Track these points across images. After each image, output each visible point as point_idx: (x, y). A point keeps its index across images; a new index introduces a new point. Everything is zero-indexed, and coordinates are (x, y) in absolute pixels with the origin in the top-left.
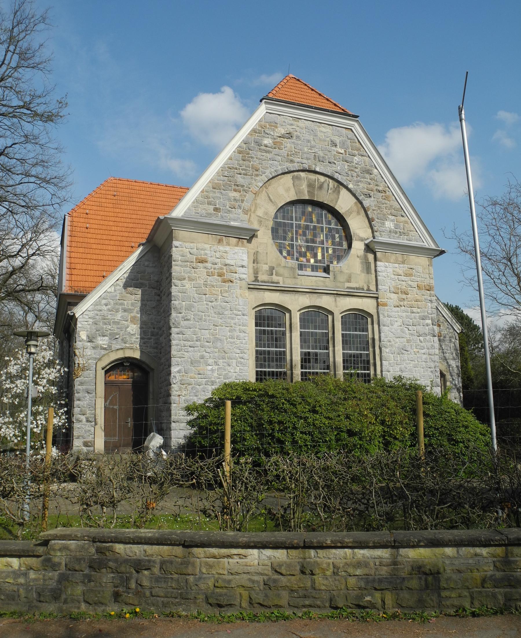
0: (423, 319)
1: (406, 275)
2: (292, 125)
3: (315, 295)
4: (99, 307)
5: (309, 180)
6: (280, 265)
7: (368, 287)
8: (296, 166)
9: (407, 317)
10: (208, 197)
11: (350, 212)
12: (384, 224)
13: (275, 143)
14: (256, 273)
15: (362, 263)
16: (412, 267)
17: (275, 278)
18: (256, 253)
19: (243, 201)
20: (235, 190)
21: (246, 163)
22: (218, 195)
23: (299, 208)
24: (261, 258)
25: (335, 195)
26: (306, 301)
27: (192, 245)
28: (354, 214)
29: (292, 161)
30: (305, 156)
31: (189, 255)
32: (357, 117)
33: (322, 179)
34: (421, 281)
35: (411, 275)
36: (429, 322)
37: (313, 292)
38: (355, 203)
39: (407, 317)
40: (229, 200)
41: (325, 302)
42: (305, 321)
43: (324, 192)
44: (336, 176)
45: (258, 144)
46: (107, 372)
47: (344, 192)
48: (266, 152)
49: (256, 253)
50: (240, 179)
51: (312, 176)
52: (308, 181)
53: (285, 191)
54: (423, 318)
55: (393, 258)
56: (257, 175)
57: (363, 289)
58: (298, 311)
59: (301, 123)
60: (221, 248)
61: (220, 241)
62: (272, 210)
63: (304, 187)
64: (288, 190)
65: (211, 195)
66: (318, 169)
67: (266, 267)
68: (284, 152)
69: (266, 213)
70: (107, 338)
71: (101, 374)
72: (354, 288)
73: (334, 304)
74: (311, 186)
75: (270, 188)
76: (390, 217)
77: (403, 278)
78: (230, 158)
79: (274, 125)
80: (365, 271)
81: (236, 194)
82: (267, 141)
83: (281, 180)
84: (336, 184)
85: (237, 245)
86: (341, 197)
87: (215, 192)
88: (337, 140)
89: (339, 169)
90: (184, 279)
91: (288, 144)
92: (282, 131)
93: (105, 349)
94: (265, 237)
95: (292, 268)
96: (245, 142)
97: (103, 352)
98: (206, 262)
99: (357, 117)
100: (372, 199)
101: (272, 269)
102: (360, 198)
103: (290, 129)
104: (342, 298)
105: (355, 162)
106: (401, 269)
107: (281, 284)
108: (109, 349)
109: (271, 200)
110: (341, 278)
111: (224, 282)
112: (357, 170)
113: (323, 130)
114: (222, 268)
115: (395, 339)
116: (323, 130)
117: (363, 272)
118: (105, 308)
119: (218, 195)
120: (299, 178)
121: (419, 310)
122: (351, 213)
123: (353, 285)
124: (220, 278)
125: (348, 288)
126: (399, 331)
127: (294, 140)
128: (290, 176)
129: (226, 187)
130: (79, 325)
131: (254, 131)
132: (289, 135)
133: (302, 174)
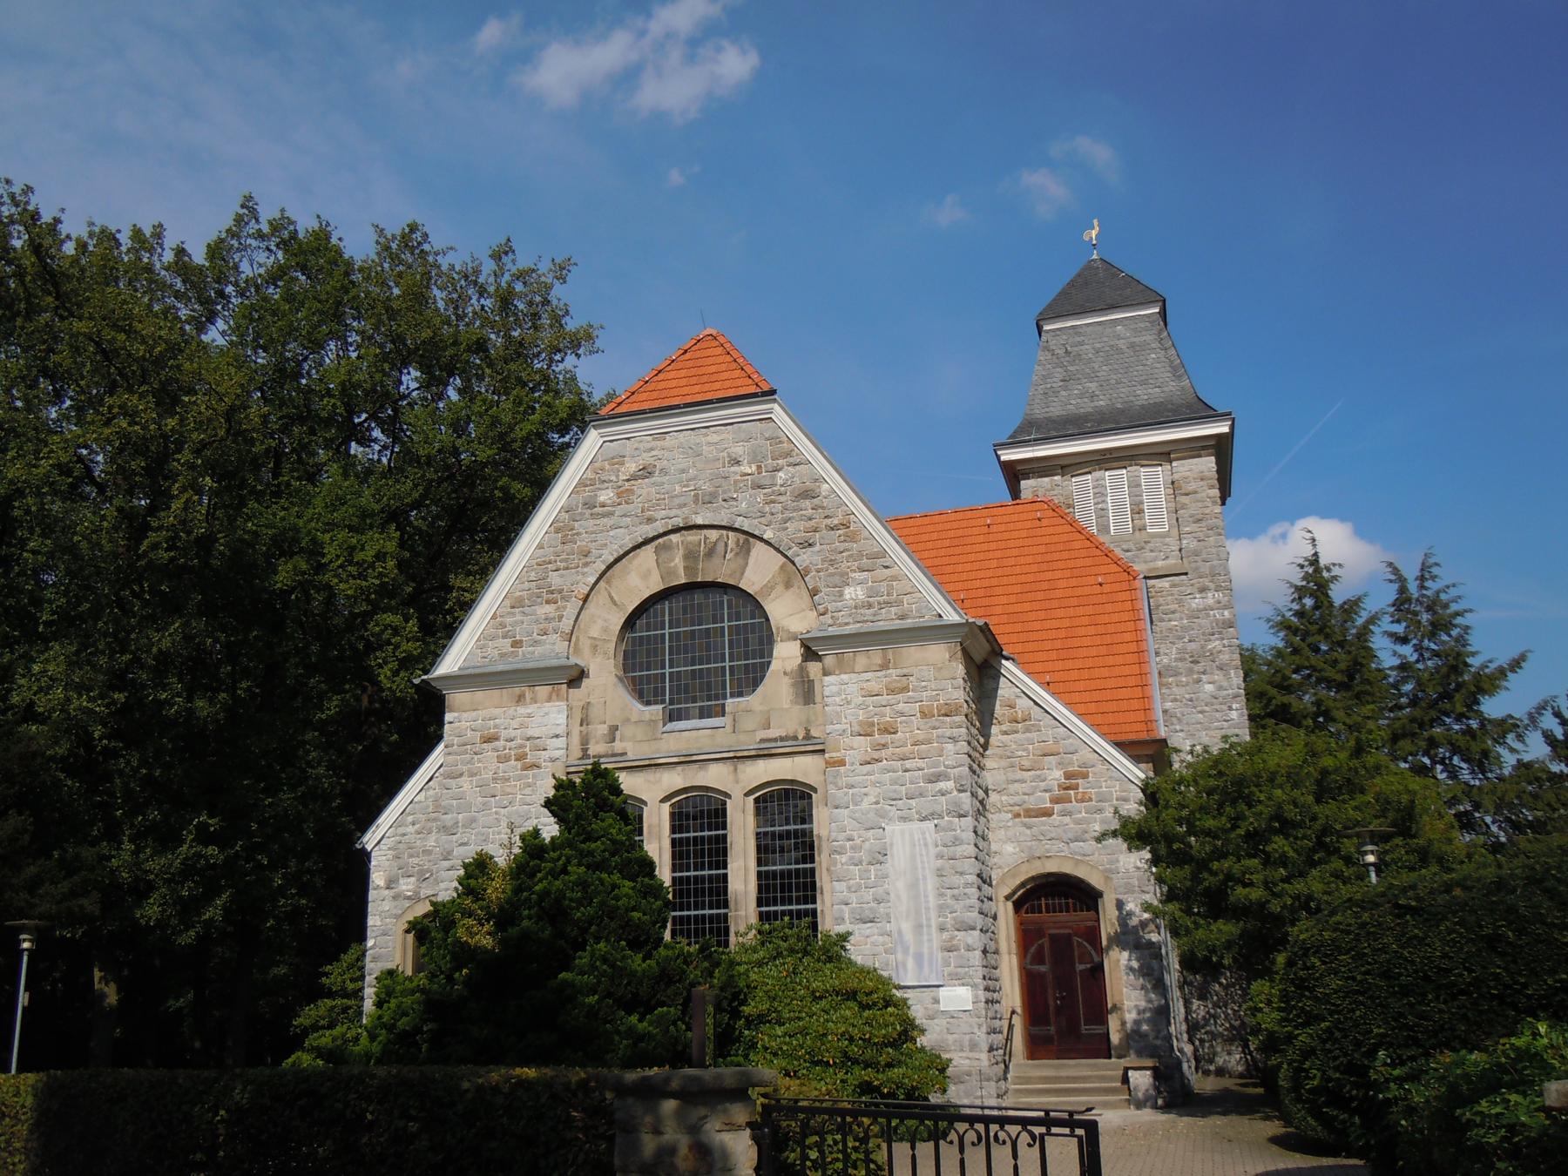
0: (931, 782)
1: (891, 691)
2: (652, 449)
3: (695, 766)
4: (401, 830)
5: (686, 545)
6: (628, 720)
7: (807, 730)
8: (659, 527)
9: (894, 782)
10: (503, 625)
11: (769, 588)
12: (841, 594)
13: (619, 495)
14: (585, 742)
15: (793, 685)
16: (905, 671)
17: (618, 746)
18: (586, 707)
19: (561, 618)
20: (548, 602)
21: (567, 547)
22: (519, 617)
23: (678, 603)
24: (595, 713)
25: (740, 561)
26: (675, 780)
27: (474, 714)
28: (780, 588)
29: (650, 520)
30: (677, 501)
31: (469, 733)
32: (773, 392)
33: (713, 535)
34: (931, 699)
35: (905, 689)
36: (950, 785)
37: (687, 761)
38: (783, 567)
39: (894, 782)
40: (537, 621)
41: (714, 776)
42: (679, 820)
43: (716, 560)
44: (739, 522)
45: (589, 505)
46: (1018, 905)
47: (758, 549)
48: (604, 515)
49: (586, 707)
50: (555, 580)
51: (692, 537)
52: (686, 548)
53: (642, 579)
54: (936, 778)
55: (861, 661)
56: (586, 565)
57: (795, 738)
58: (662, 801)
59: (669, 441)
60: (521, 710)
61: (520, 699)
62: (618, 620)
63: (678, 562)
64: (646, 576)
65: (509, 620)
66: (700, 521)
67: (602, 729)
68: (635, 507)
69: (605, 630)
70: (413, 879)
71: (1006, 912)
72: (775, 740)
73: (731, 777)
74: (691, 556)
75: (615, 582)
76: (856, 575)
77: (884, 699)
78: (540, 546)
79: (618, 460)
80: (801, 700)
81: (549, 609)
82: (606, 496)
83: (636, 562)
84: (742, 537)
85: (549, 700)
86: (751, 560)
87: (514, 614)
88: (738, 450)
89: (743, 509)
90: (461, 775)
91: (644, 489)
92: (632, 467)
93: (409, 898)
94: (604, 674)
95: (652, 722)
96: (567, 509)
97: (407, 904)
98: (497, 739)
99: (773, 392)
100: (817, 548)
101: (614, 729)
102: (789, 554)
103: (646, 458)
104: (749, 762)
105: (780, 482)
106: (875, 681)
107: (630, 756)
108: (415, 899)
109: (615, 603)
110: (748, 723)
111: (525, 768)
112: (782, 499)
113: (714, 438)
114: (522, 746)
115: (862, 832)
116: (714, 438)
117: (797, 703)
118: (411, 829)
119: (519, 617)
120: (667, 547)
121: (921, 763)
122: (772, 588)
123: (773, 733)
124: (519, 764)
125: (763, 741)
126: (871, 815)
127: (656, 478)
128: (650, 548)
129: (535, 599)
130: (373, 863)
131: (582, 484)
132: (646, 472)
133: (674, 538)
